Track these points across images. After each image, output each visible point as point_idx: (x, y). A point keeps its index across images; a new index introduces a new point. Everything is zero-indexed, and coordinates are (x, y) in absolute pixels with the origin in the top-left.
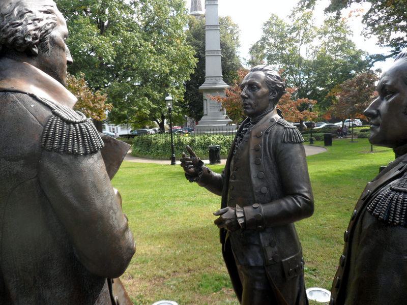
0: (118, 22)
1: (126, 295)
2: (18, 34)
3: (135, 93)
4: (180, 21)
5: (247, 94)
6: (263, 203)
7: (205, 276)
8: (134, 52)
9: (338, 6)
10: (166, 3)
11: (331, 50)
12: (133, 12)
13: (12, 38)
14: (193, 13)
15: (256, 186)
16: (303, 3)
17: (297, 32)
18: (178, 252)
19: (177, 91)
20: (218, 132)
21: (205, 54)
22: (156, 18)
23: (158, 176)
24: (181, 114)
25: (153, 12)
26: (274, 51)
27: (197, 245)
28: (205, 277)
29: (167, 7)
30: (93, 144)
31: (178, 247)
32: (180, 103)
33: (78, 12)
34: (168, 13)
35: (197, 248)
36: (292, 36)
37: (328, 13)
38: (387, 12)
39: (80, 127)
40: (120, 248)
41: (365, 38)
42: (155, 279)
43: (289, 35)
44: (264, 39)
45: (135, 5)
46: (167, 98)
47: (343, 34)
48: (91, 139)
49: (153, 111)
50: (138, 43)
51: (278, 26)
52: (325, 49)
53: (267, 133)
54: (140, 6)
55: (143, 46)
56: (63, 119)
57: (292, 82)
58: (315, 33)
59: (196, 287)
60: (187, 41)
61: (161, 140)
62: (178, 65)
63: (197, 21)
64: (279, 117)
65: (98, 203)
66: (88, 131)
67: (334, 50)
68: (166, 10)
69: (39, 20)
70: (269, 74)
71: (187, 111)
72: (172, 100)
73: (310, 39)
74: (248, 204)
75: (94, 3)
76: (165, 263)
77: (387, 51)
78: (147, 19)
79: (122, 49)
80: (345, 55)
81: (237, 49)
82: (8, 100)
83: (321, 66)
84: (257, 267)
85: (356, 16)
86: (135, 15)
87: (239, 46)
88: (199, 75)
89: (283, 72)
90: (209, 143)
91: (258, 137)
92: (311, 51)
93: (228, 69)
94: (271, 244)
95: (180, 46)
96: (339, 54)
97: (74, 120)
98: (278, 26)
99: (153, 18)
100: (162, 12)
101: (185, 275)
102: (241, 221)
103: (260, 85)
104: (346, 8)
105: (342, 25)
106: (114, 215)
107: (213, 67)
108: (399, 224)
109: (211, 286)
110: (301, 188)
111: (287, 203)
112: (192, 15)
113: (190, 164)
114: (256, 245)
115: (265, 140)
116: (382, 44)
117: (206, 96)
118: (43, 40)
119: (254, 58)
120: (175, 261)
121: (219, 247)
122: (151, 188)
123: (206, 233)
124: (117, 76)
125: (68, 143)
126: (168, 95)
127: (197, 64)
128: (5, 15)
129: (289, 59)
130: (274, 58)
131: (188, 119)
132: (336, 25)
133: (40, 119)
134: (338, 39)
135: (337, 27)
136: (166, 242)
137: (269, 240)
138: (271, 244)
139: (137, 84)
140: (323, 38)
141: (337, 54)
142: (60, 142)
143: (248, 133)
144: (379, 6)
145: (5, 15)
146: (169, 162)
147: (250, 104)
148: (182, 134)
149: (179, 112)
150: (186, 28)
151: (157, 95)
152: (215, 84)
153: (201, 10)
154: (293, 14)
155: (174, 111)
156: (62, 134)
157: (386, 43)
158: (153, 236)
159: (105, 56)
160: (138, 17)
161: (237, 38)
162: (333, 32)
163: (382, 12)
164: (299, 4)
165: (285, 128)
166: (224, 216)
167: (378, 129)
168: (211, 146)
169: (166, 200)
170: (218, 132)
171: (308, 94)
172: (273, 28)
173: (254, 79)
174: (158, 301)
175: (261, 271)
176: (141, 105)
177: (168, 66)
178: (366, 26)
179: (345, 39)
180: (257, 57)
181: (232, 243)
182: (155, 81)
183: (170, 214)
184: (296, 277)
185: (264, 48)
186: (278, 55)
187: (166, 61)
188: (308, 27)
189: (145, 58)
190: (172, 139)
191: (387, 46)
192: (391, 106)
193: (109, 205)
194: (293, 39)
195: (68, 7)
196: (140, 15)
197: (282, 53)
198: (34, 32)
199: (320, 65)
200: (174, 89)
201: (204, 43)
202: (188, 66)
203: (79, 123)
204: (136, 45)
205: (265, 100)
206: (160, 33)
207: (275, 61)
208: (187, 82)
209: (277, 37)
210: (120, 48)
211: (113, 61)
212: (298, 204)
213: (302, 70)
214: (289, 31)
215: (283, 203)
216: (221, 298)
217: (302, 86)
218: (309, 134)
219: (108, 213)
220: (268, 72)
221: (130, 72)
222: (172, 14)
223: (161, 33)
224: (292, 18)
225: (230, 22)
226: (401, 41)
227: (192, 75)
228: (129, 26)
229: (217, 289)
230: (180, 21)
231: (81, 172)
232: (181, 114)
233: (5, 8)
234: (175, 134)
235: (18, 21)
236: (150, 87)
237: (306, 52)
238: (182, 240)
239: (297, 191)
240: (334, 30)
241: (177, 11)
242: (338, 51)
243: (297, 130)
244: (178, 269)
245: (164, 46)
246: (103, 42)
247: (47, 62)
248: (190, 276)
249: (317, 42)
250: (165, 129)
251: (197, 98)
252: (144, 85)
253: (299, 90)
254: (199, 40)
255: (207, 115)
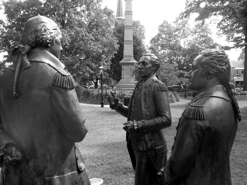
0: (73, 22)
1: (81, 156)
2: (44, 39)
3: (81, 64)
4: (109, 22)
5: (141, 67)
6: (147, 120)
7: (119, 167)
8: (82, 39)
9: (203, 17)
10: (102, 12)
11: (199, 42)
12: (82, 16)
13: (41, 40)
14: (118, 18)
15: (144, 111)
16: (182, 15)
17: (179, 31)
18: (103, 155)
19: (106, 64)
20: (130, 89)
21: (123, 42)
22: (96, 20)
23: (93, 113)
24: (108, 77)
25: (94, 17)
26: (165, 42)
27: (114, 151)
28: (118, 167)
29: (102, 14)
30: (73, 85)
31: (104, 152)
32: (107, 71)
33: (50, 15)
34: (103, 17)
35: (115, 152)
36: (175, 34)
37: (197, 21)
38: (232, 21)
39: (68, 77)
40: (82, 129)
41: (219, 37)
42: (91, 168)
43: (174, 33)
44: (159, 35)
45: (83, 12)
46: (100, 68)
47: (206, 33)
48: (72, 83)
49: (92, 75)
50: (84, 34)
51: (168, 27)
52: (195, 42)
53: (150, 86)
54: (87, 12)
55: (87, 36)
56: (62, 74)
57: (175, 61)
58: (189, 32)
59: (113, 172)
60: (113, 34)
61: (96, 92)
62: (108, 48)
63: (120, 23)
64: (157, 79)
65: (74, 109)
66: (71, 80)
67: (200, 43)
68: (102, 16)
69: (52, 33)
70: (152, 58)
71: (112, 76)
72: (103, 69)
73: (187, 36)
74: (140, 120)
75: (59, 10)
76: (97, 160)
77: (231, 44)
78: (90, 20)
79: (75, 38)
80: (207, 46)
81: (143, 40)
82: (39, 66)
83: (193, 52)
84: (144, 151)
85: (214, 23)
86: (83, 17)
87: (144, 38)
88: (120, 55)
89: (170, 55)
90: (124, 95)
91: (146, 88)
92: (187, 43)
93: (137, 52)
94: (151, 140)
95: (109, 37)
96: (203, 45)
97: (65, 74)
98: (168, 27)
99: (94, 20)
100: (99, 17)
101: (107, 166)
102: (136, 128)
103: (148, 63)
104: (208, 18)
105: (205, 28)
106: (80, 115)
107: (128, 50)
108: (192, 118)
109: (122, 171)
110: (165, 113)
111: (158, 120)
112: (117, 19)
113: (112, 100)
114: (143, 140)
115: (149, 90)
116: (229, 41)
117: (124, 67)
118: (53, 41)
119: (153, 46)
120: (102, 159)
121: (127, 153)
122: (89, 120)
123: (120, 145)
124: (71, 53)
125: (63, 85)
126: (101, 66)
127: (119, 48)
128: (39, 30)
129: (173, 46)
130: (165, 46)
131: (112, 80)
132: (202, 28)
133: (52, 74)
134: (203, 36)
135: (202, 29)
136: (97, 149)
137: (150, 138)
138: (151, 140)
139: (82, 58)
140: (194, 36)
141: (202, 45)
142: (61, 83)
143: (142, 86)
144: (227, 18)
145: (39, 30)
146: (100, 106)
147: (143, 72)
148: (108, 89)
149: (107, 76)
150: (113, 27)
151: (94, 66)
152: (129, 60)
153: (123, 16)
154: (177, 21)
155: (104, 75)
156: (61, 80)
157: (231, 40)
158: (89, 146)
159: (65, 41)
160: (85, 19)
161: (143, 34)
162: (200, 32)
163: (229, 21)
164: (180, 15)
165: (159, 84)
166: (128, 125)
167: (190, 83)
168: (126, 97)
169: (98, 127)
170: (130, 89)
171: (184, 68)
172: (164, 29)
173: (145, 60)
174: (92, 178)
175: (146, 153)
176: (84, 71)
177: (101, 48)
178: (219, 29)
179: (207, 37)
180: (155, 45)
181: (131, 140)
182: (93, 57)
183: (99, 134)
184: (163, 157)
185: (159, 40)
186: (167, 45)
187: (100, 46)
188: (185, 29)
189: (88, 43)
190: (102, 92)
191: (232, 41)
192: (195, 73)
193: (78, 110)
194: (176, 35)
195: (44, 12)
196: (86, 18)
197: (170, 44)
198: (50, 38)
199: (193, 51)
200: (105, 63)
201: (123, 36)
202: (113, 49)
203: (68, 76)
204: (83, 36)
205: (150, 70)
206: (97, 29)
207: (166, 48)
208: (112, 58)
209: (166, 36)
210: (73, 37)
211: (69, 44)
212: (163, 120)
213: (181, 54)
214: (174, 31)
215: (156, 120)
216: (127, 178)
217: (181, 63)
218: (184, 92)
219: (78, 114)
220: (152, 57)
221: (79, 51)
222: (105, 18)
223: (98, 29)
224: (176, 24)
225: (139, 24)
226: (240, 39)
227: (115, 55)
228: (79, 24)
229: (125, 173)
230: (109, 22)
231: (68, 96)
232: (108, 77)
233: (39, 28)
234: (104, 89)
235: (44, 34)
236: (90, 60)
237: (184, 43)
238: (106, 148)
239: (164, 114)
240: (201, 31)
241: (108, 16)
242: (202, 44)
243: (165, 85)
244: (103, 163)
245: (99, 37)
246: (63, 33)
247: (53, 50)
248: (110, 166)
249: (190, 38)
250: (98, 86)
251: (118, 68)
252: (87, 59)
253: (179, 66)
254: (121, 34)
255: (123, 78)
